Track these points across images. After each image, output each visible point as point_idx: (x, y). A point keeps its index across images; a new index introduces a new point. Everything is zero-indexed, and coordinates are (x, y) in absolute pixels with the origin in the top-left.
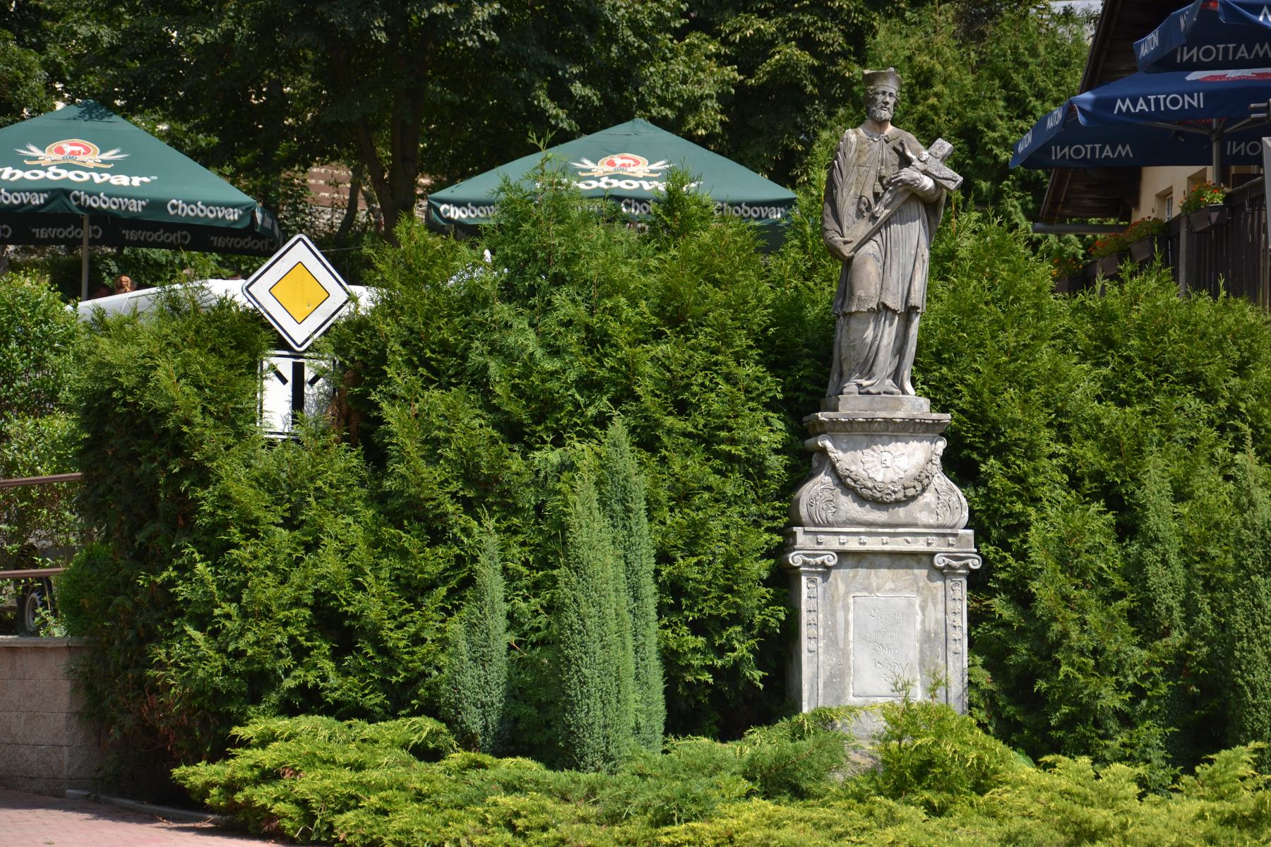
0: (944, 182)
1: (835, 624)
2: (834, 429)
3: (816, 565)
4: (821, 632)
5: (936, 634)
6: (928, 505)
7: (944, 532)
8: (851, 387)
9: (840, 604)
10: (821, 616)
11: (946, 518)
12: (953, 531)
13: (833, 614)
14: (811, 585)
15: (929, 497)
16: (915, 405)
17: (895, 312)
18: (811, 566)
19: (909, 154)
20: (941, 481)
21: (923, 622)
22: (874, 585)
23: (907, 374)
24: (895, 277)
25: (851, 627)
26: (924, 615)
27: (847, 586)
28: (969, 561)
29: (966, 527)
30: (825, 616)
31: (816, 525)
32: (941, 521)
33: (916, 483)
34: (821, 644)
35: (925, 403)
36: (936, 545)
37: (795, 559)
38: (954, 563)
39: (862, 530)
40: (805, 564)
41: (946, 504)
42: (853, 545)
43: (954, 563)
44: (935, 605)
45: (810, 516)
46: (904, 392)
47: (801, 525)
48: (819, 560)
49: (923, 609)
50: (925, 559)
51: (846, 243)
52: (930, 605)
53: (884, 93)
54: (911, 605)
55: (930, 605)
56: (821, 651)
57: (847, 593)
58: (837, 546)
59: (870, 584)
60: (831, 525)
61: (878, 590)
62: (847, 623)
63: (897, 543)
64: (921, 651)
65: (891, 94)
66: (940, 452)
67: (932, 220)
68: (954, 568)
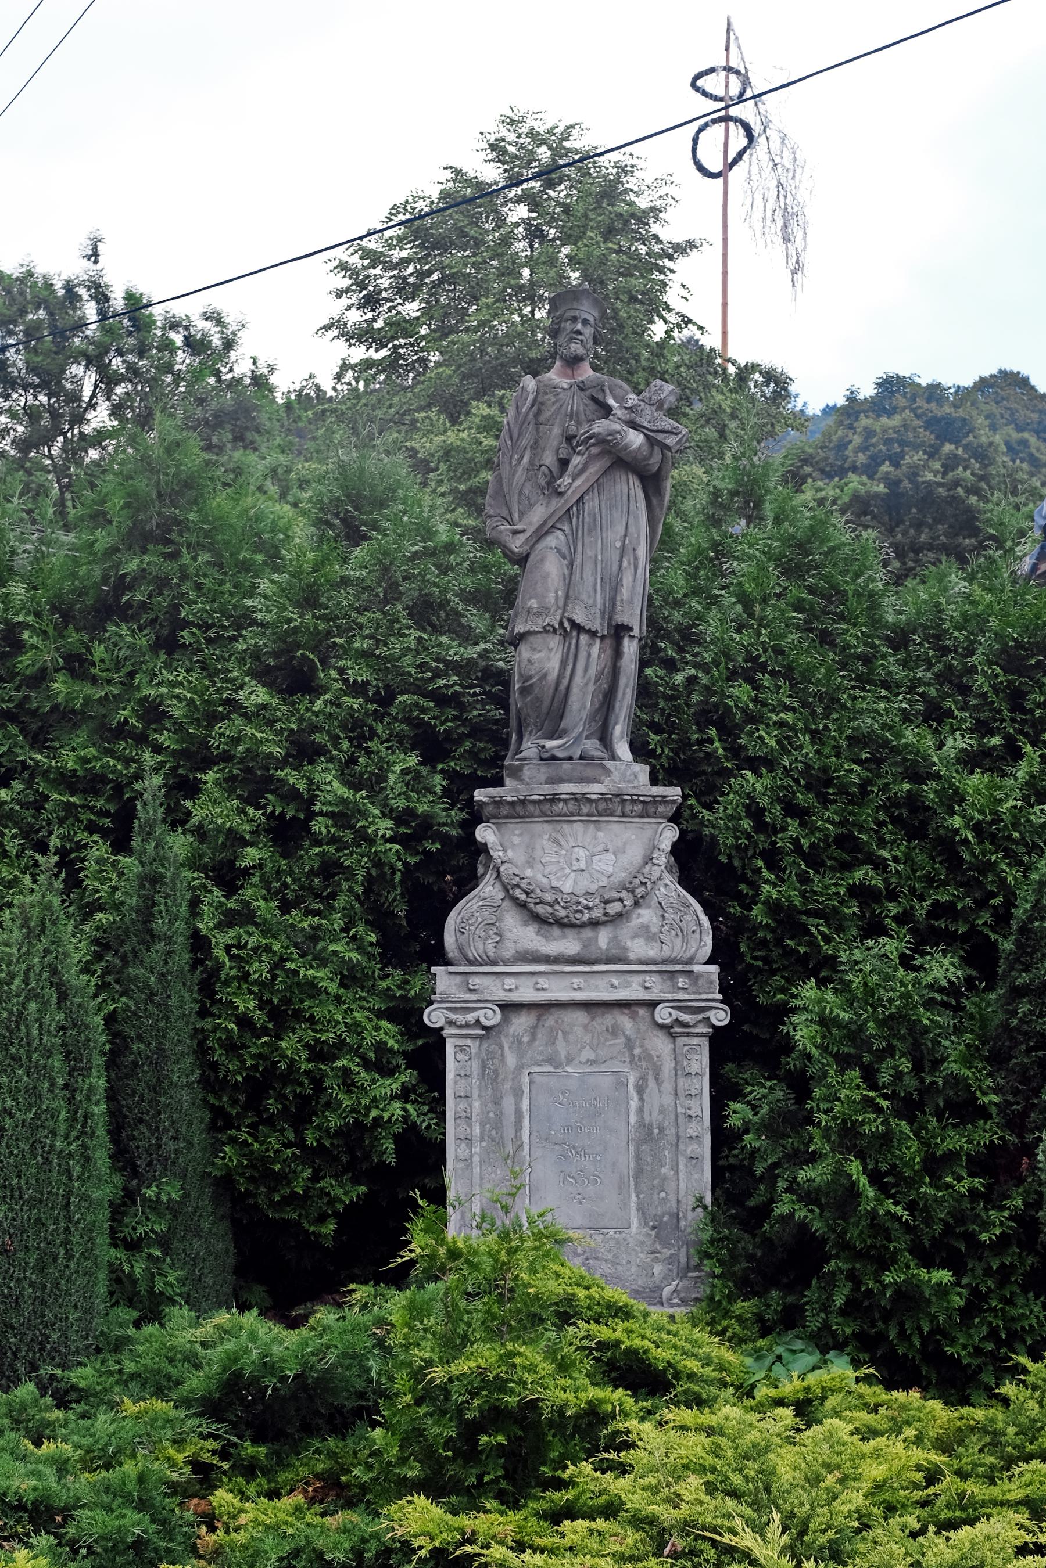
0: (660, 437)
1: (500, 1117)
2: (519, 811)
3: (467, 1026)
4: (477, 1130)
5: (661, 1130)
6: (645, 928)
7: (670, 970)
8: (530, 748)
9: (508, 1085)
10: (476, 1104)
11: (674, 947)
12: (688, 968)
13: (497, 1102)
14: (461, 1056)
15: (646, 916)
16: (629, 774)
17: (593, 634)
18: (461, 1027)
19: (611, 402)
20: (670, 889)
21: (640, 1110)
22: (563, 1054)
23: (620, 731)
24: (589, 581)
25: (526, 1122)
26: (641, 1099)
27: (520, 1056)
28: (711, 1014)
29: (707, 963)
30: (484, 1105)
31: (471, 963)
32: (667, 952)
33: (624, 894)
34: (477, 1149)
35: (642, 771)
36: (658, 989)
37: (434, 1017)
38: (686, 1017)
39: (542, 968)
40: (451, 1023)
41: (677, 929)
42: (526, 993)
43: (686, 1017)
44: (659, 1082)
45: (461, 950)
46: (614, 757)
47: (448, 963)
48: (471, 1017)
49: (640, 1090)
50: (642, 1012)
51: (515, 532)
52: (652, 1083)
53: (574, 319)
54: (621, 1084)
55: (652, 1083)
56: (476, 1159)
57: (519, 1068)
58: (502, 996)
59: (556, 1052)
60: (495, 963)
61: (569, 1061)
62: (519, 1114)
63: (597, 989)
64: (638, 1157)
65: (585, 322)
66: (666, 844)
67: (654, 501)
68: (686, 1025)
